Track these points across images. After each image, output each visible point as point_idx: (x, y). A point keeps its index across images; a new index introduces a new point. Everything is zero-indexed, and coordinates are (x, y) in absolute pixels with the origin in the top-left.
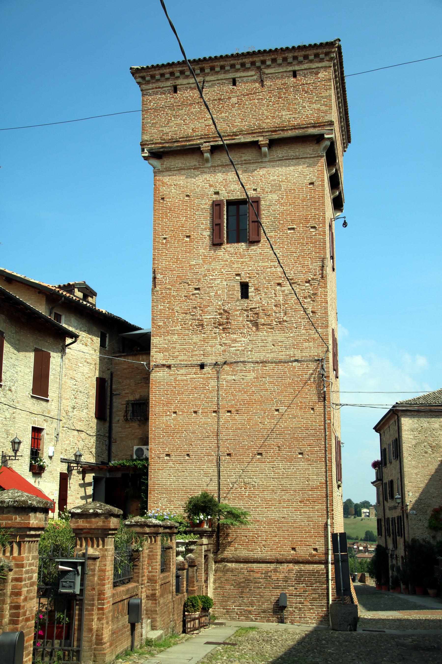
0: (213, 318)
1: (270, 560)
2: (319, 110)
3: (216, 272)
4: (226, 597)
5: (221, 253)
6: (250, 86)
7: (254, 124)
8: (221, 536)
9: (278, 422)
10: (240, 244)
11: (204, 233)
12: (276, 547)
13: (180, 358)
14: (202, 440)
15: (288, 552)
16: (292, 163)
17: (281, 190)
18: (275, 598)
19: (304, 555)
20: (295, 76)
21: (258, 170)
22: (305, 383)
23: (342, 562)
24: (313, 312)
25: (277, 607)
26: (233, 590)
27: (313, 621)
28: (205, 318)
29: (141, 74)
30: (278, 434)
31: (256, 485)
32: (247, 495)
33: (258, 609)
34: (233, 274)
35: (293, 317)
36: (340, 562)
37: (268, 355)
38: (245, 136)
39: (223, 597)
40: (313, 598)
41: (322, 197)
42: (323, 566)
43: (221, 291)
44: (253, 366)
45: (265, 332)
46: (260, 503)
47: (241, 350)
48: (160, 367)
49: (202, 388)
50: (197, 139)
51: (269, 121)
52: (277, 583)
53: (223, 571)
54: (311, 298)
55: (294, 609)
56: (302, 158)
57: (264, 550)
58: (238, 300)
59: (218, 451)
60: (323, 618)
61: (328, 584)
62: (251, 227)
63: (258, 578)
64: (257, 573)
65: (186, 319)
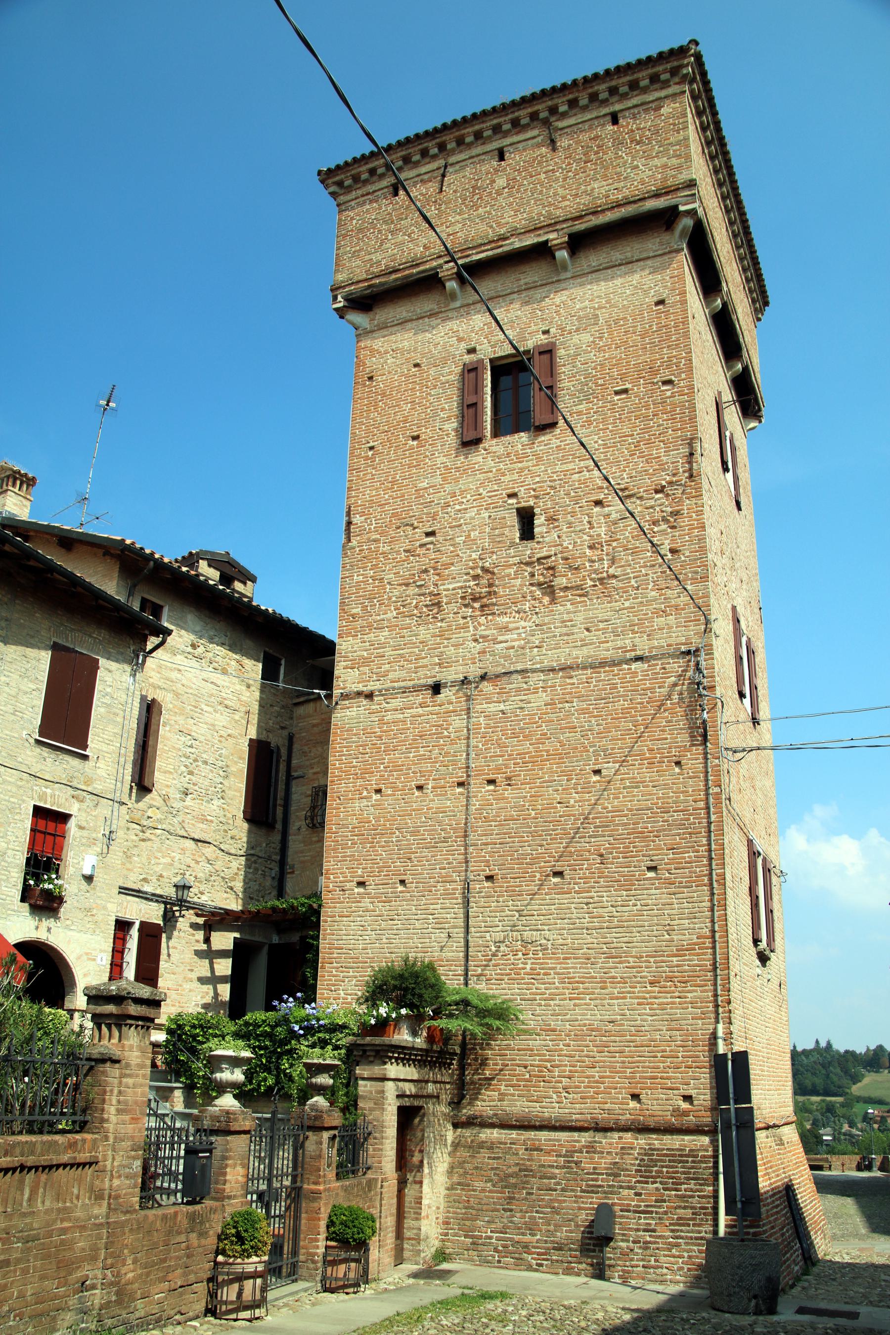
0: (461, 588)
1: (579, 1124)
2: (665, 166)
3: (468, 496)
4: (472, 1208)
5: (478, 457)
6: (528, 155)
7: (540, 214)
8: (470, 1064)
9: (598, 799)
10: (516, 436)
11: (446, 427)
12: (594, 1092)
13: (391, 676)
14: (433, 847)
15: (622, 1103)
16: (618, 273)
17: (597, 324)
18: (587, 1215)
19: (660, 1113)
20: (615, 121)
21: (552, 296)
22: (660, 707)
23: (737, 1127)
24: (673, 551)
25: (590, 1238)
26: (490, 1191)
27: (678, 1277)
28: (445, 590)
29: (337, 179)
30: (599, 827)
31: (550, 946)
32: (528, 970)
33: (546, 1242)
34: (502, 494)
35: (630, 565)
36: (734, 1128)
37: (575, 653)
38: (521, 237)
39: (466, 1208)
40: (679, 1219)
41: (682, 322)
42: (706, 1140)
43: (477, 533)
44: (542, 678)
45: (568, 603)
46: (557, 988)
47: (519, 647)
48: (351, 698)
49: (434, 734)
50: (431, 260)
51: (568, 203)
52: (593, 1180)
53: (470, 1147)
54: (668, 521)
55: (631, 1244)
56: (637, 261)
57: (566, 1098)
58: (513, 544)
59: (466, 871)
60: (703, 1271)
61: (718, 1185)
62: (537, 400)
63: (550, 1166)
64: (548, 1153)
65: (406, 596)
